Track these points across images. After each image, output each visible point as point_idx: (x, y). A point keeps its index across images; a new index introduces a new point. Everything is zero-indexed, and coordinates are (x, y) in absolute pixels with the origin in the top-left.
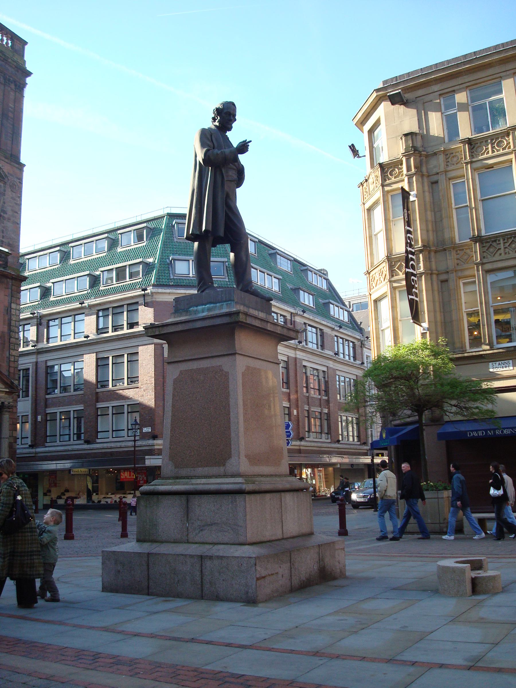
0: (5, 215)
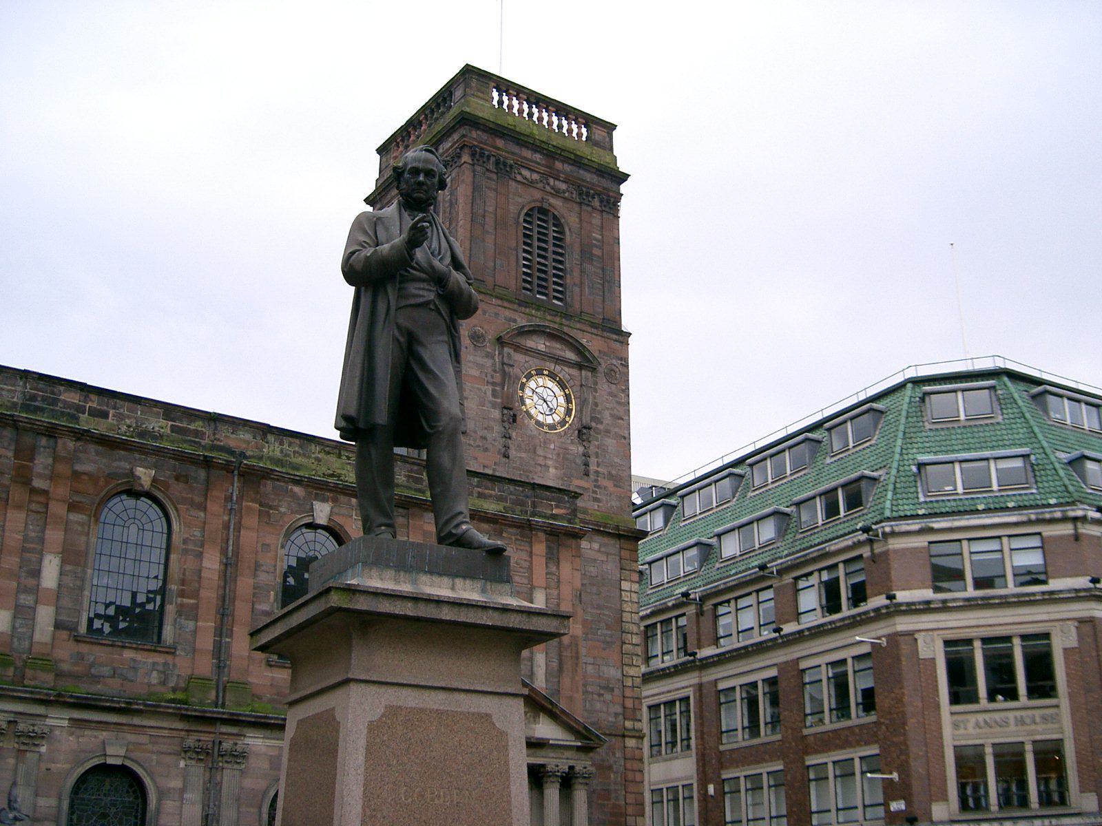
0: (599, 426)
